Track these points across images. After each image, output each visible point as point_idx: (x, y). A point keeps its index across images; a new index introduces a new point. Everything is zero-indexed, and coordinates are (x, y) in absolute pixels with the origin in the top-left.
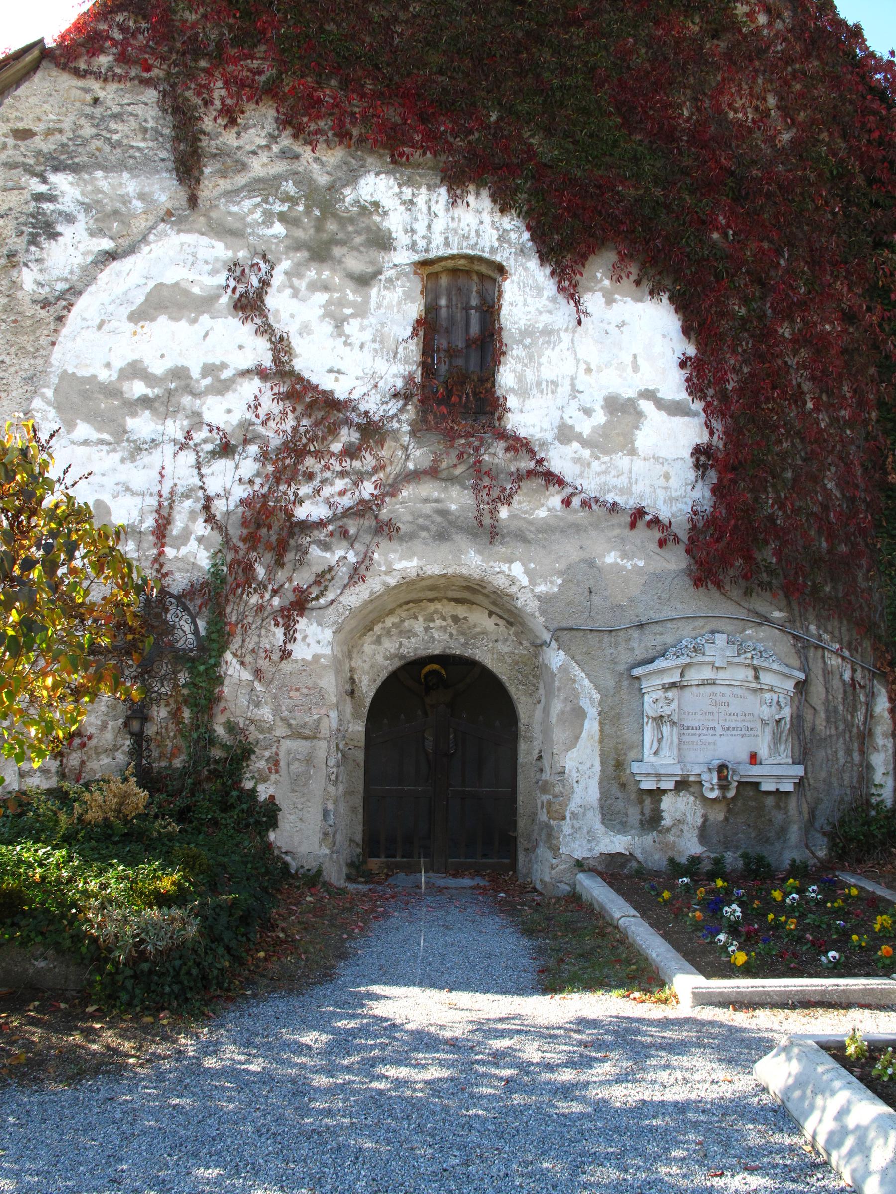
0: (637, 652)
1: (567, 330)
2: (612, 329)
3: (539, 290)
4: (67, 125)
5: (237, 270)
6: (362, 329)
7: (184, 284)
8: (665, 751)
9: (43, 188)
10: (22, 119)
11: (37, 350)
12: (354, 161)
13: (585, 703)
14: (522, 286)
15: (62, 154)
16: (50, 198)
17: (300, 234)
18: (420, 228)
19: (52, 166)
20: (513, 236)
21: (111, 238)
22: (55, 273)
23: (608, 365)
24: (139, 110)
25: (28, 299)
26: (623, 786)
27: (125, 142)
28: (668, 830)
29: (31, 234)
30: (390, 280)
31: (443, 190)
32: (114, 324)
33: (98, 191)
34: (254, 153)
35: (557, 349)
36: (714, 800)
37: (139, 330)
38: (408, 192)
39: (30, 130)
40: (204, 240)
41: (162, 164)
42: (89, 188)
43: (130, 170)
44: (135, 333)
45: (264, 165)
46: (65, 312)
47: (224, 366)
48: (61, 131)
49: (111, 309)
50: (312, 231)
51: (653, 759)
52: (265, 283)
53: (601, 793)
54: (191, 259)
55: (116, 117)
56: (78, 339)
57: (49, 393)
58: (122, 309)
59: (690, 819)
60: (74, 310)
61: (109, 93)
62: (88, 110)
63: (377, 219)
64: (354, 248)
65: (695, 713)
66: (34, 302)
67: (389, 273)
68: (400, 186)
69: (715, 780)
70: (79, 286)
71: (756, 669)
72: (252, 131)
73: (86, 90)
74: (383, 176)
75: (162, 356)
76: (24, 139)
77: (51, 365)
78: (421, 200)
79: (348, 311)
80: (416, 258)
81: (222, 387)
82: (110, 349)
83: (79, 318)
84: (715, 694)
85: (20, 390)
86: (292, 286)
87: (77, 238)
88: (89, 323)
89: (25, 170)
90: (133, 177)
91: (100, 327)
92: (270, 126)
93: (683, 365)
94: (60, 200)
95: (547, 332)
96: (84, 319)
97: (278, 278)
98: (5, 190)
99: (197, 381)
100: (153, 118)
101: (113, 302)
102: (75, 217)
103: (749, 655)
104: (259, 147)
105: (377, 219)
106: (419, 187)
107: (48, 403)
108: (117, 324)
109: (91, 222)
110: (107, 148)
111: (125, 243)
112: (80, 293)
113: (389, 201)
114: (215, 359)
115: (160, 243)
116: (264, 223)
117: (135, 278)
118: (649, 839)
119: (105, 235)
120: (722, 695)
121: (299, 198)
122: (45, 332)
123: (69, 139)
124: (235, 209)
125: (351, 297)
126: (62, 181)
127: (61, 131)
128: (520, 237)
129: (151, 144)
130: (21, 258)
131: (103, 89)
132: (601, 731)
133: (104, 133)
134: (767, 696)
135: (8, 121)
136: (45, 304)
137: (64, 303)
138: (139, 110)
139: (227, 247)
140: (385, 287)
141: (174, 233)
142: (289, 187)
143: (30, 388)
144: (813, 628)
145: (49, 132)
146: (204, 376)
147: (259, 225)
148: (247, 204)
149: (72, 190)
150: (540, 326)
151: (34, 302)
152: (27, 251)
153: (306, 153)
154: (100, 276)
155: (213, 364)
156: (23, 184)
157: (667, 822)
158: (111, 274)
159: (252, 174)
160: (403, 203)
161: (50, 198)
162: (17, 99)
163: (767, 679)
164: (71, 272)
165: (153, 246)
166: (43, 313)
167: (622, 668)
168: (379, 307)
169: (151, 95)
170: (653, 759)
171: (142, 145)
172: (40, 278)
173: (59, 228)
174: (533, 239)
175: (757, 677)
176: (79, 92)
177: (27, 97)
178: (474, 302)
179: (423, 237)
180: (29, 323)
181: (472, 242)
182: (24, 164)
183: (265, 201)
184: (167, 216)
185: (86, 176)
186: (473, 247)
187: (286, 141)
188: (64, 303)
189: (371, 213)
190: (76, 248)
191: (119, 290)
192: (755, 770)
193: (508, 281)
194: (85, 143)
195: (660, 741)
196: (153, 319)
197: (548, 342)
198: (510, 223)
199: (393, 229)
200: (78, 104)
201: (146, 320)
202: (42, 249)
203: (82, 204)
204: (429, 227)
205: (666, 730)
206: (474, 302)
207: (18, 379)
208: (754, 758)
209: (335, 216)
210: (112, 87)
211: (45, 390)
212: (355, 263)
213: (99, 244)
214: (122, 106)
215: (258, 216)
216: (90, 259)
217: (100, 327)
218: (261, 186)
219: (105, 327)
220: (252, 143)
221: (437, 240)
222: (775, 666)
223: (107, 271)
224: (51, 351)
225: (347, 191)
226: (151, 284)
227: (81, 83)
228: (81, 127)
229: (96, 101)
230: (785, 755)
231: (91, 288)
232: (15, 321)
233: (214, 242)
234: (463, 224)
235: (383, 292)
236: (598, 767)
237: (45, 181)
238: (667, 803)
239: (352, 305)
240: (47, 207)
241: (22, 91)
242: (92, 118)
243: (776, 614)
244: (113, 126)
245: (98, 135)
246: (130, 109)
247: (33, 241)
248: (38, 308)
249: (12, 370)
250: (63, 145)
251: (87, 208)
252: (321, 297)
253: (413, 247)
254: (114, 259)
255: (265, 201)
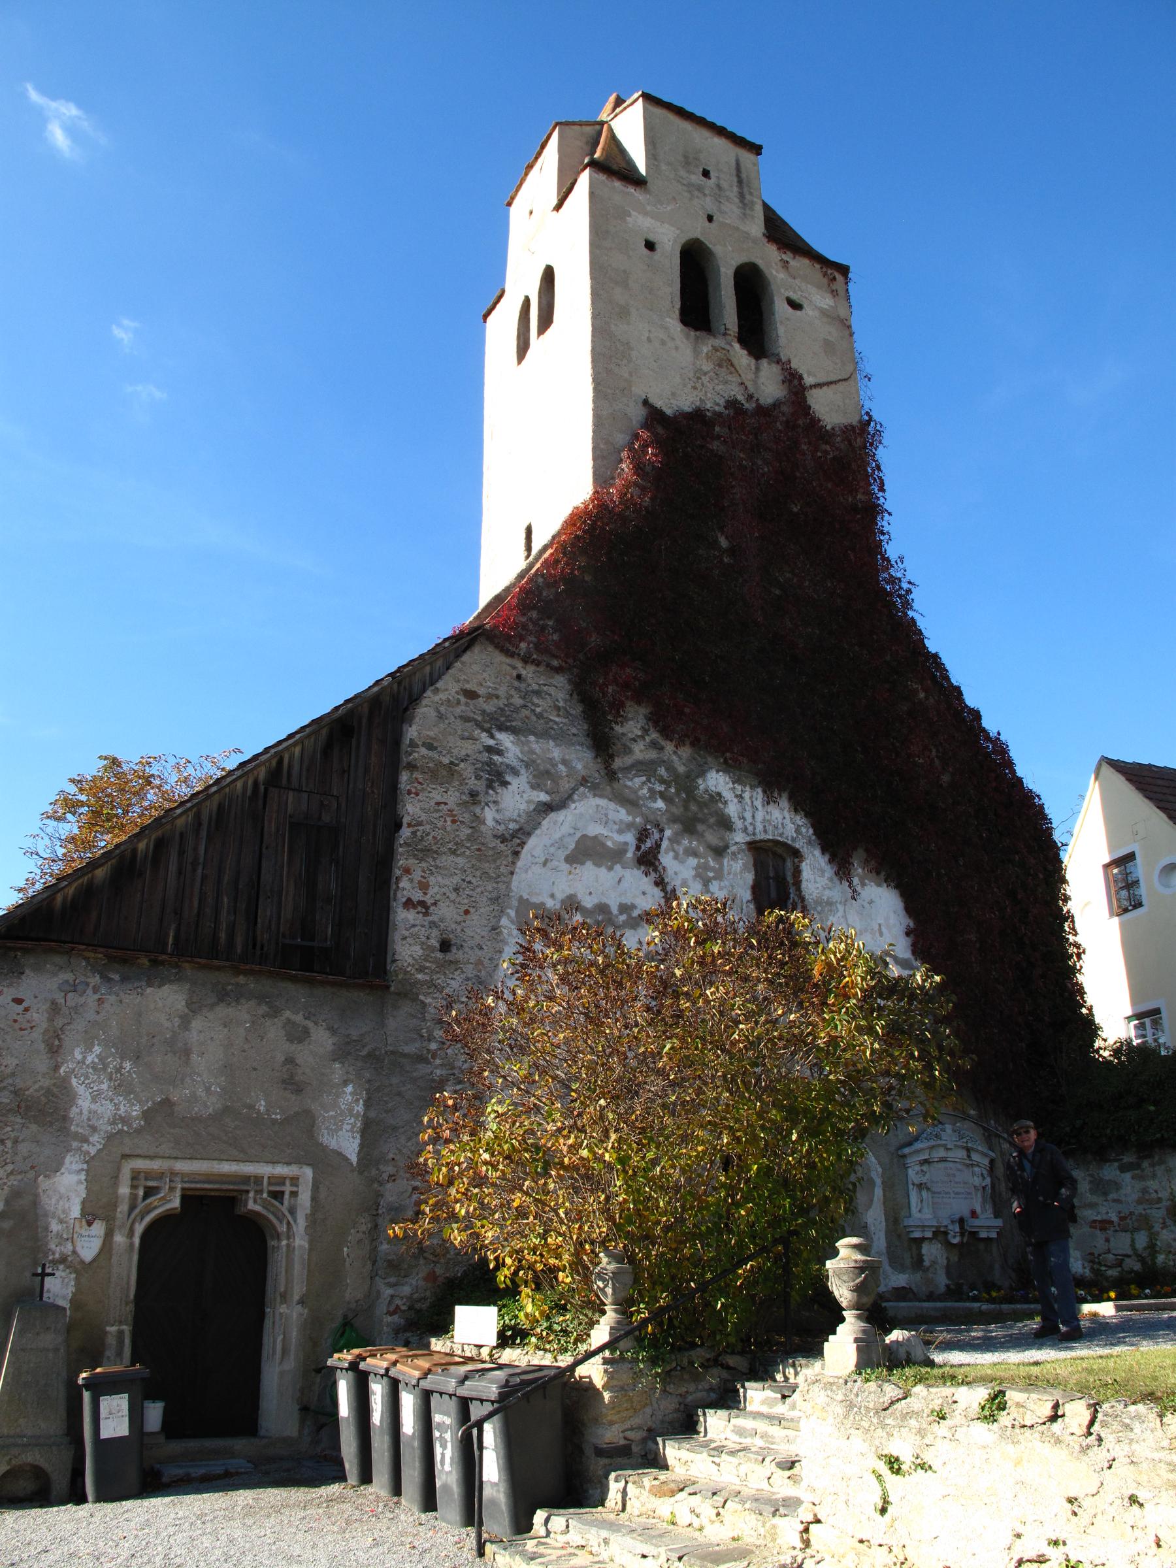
0: (900, 1137)
1: (840, 903)
2: (866, 905)
3: (823, 871)
4: (502, 692)
5: (643, 835)
6: (721, 889)
7: (603, 839)
8: (925, 1210)
9: (491, 742)
10: (468, 682)
11: (499, 876)
12: (699, 759)
13: (873, 1175)
14: (813, 868)
15: (502, 716)
16: (499, 752)
17: (674, 810)
18: (748, 815)
19: (496, 725)
20: (804, 830)
21: (547, 793)
22: (508, 814)
23: (866, 930)
24: (552, 690)
25: (490, 832)
26: (899, 1236)
27: (545, 715)
28: (928, 1269)
29: (487, 779)
30: (734, 854)
31: (759, 790)
32: (555, 863)
33: (532, 752)
34: (634, 740)
35: (836, 916)
36: (955, 1245)
37: (573, 871)
38: (739, 787)
39: (475, 692)
40: (612, 805)
41: (575, 739)
42: (526, 748)
43: (554, 739)
44: (570, 873)
45: (641, 751)
46: (519, 849)
47: (633, 907)
48: (497, 697)
49: (552, 850)
50: (682, 809)
51: (918, 1215)
52: (658, 846)
53: (887, 1242)
54: (604, 819)
55: (537, 693)
56: (530, 872)
57: (512, 913)
58: (560, 851)
59: (940, 1261)
60: (526, 848)
61: (528, 671)
62: (516, 683)
63: (720, 805)
64: (710, 827)
65: (937, 1182)
66: (495, 836)
67: (733, 848)
68: (733, 783)
69: (957, 1230)
70: (527, 828)
71: (968, 1150)
72: (631, 723)
73: (514, 668)
74: (721, 773)
75: (590, 893)
76: (472, 699)
77: (512, 891)
78: (747, 795)
79: (711, 874)
80: (748, 839)
81: (634, 923)
82: (553, 883)
83: (529, 855)
84: (946, 1168)
85: (488, 908)
86: (674, 850)
87: (522, 789)
88: (537, 860)
89: (476, 725)
90: (557, 745)
91: (545, 864)
92: (642, 722)
93: (907, 934)
94: (506, 755)
95: (830, 903)
96: (533, 856)
97: (665, 844)
98: (463, 739)
99: (617, 916)
100: (563, 700)
101: (552, 845)
102: (518, 771)
103: (965, 1140)
104: (638, 736)
105: (720, 805)
106: (745, 786)
107: (512, 922)
108: (557, 863)
109: (531, 777)
110: (534, 718)
111: (557, 798)
112: (529, 834)
113: (727, 795)
114: (628, 900)
115: (582, 803)
116: (650, 798)
117: (566, 829)
118: (918, 1276)
119: (542, 790)
120: (951, 1169)
121: (670, 782)
122: (504, 862)
123: (506, 705)
124: (629, 783)
125: (712, 863)
126: (505, 740)
127: (497, 697)
128: (807, 831)
129: (564, 721)
130: (481, 797)
131: (525, 668)
132: (884, 1195)
133: (529, 704)
134: (976, 1169)
135: (459, 681)
136: (504, 840)
137: (518, 841)
138: (552, 690)
139: (629, 813)
140: (732, 859)
141: (591, 796)
142: (662, 771)
143: (496, 908)
144: (992, 1122)
145: (490, 697)
146: (621, 913)
147: (647, 799)
148: (638, 781)
149: (513, 748)
150: (825, 898)
151: (495, 836)
152: (487, 793)
153: (669, 747)
154: (544, 823)
155: (626, 904)
156: (476, 736)
157: (927, 1263)
158: (549, 823)
159: (635, 757)
160: (736, 796)
161: (499, 752)
162: (463, 663)
163: (975, 1157)
164: (519, 816)
165: (577, 804)
166: (502, 847)
167: (892, 1149)
168: (729, 873)
169: (561, 680)
170: (918, 1215)
171: (557, 719)
172: (498, 817)
173: (508, 778)
174: (815, 833)
175: (969, 1156)
176: (508, 668)
177: (471, 664)
178: (771, 874)
179: (751, 824)
180: (491, 853)
181: (780, 831)
182: (475, 720)
183: (649, 780)
184: (584, 781)
185: (523, 739)
186: (781, 835)
187: (654, 735)
188: (518, 841)
189: (717, 801)
190: (522, 796)
191: (557, 836)
192: (977, 1222)
193: (804, 863)
194: (517, 710)
195: (922, 1201)
196: (583, 863)
197: (831, 911)
198: (800, 820)
199: (732, 815)
200: (508, 678)
201: (577, 863)
202: (497, 793)
203: (522, 761)
204: (753, 817)
205: (924, 1193)
206: (771, 874)
207: (485, 899)
208: (974, 1214)
209: (695, 800)
210: (531, 668)
211: (509, 911)
212: (712, 838)
213: (538, 796)
214: (540, 685)
215: (645, 791)
216: (532, 807)
217: (545, 864)
218: (644, 768)
219: (548, 864)
220: (632, 732)
221: (759, 828)
222: (980, 1148)
223: (547, 819)
224: (511, 879)
225: (700, 781)
226: (578, 835)
227: (509, 660)
228: (512, 696)
229: (519, 677)
230: (989, 1213)
231: (538, 832)
232: (479, 850)
233: (620, 809)
234: (773, 818)
235: (732, 863)
236: (884, 1224)
237: (492, 737)
238: (926, 1249)
239: (712, 869)
240: (496, 758)
241: (466, 657)
242: (520, 691)
243: (972, 1112)
244: (536, 700)
245: (525, 706)
246: (545, 688)
247: (490, 785)
248: (498, 841)
249: (479, 890)
250: (502, 710)
251: (527, 766)
252: (693, 862)
253: (745, 830)
254: (552, 810)
255: (649, 780)
